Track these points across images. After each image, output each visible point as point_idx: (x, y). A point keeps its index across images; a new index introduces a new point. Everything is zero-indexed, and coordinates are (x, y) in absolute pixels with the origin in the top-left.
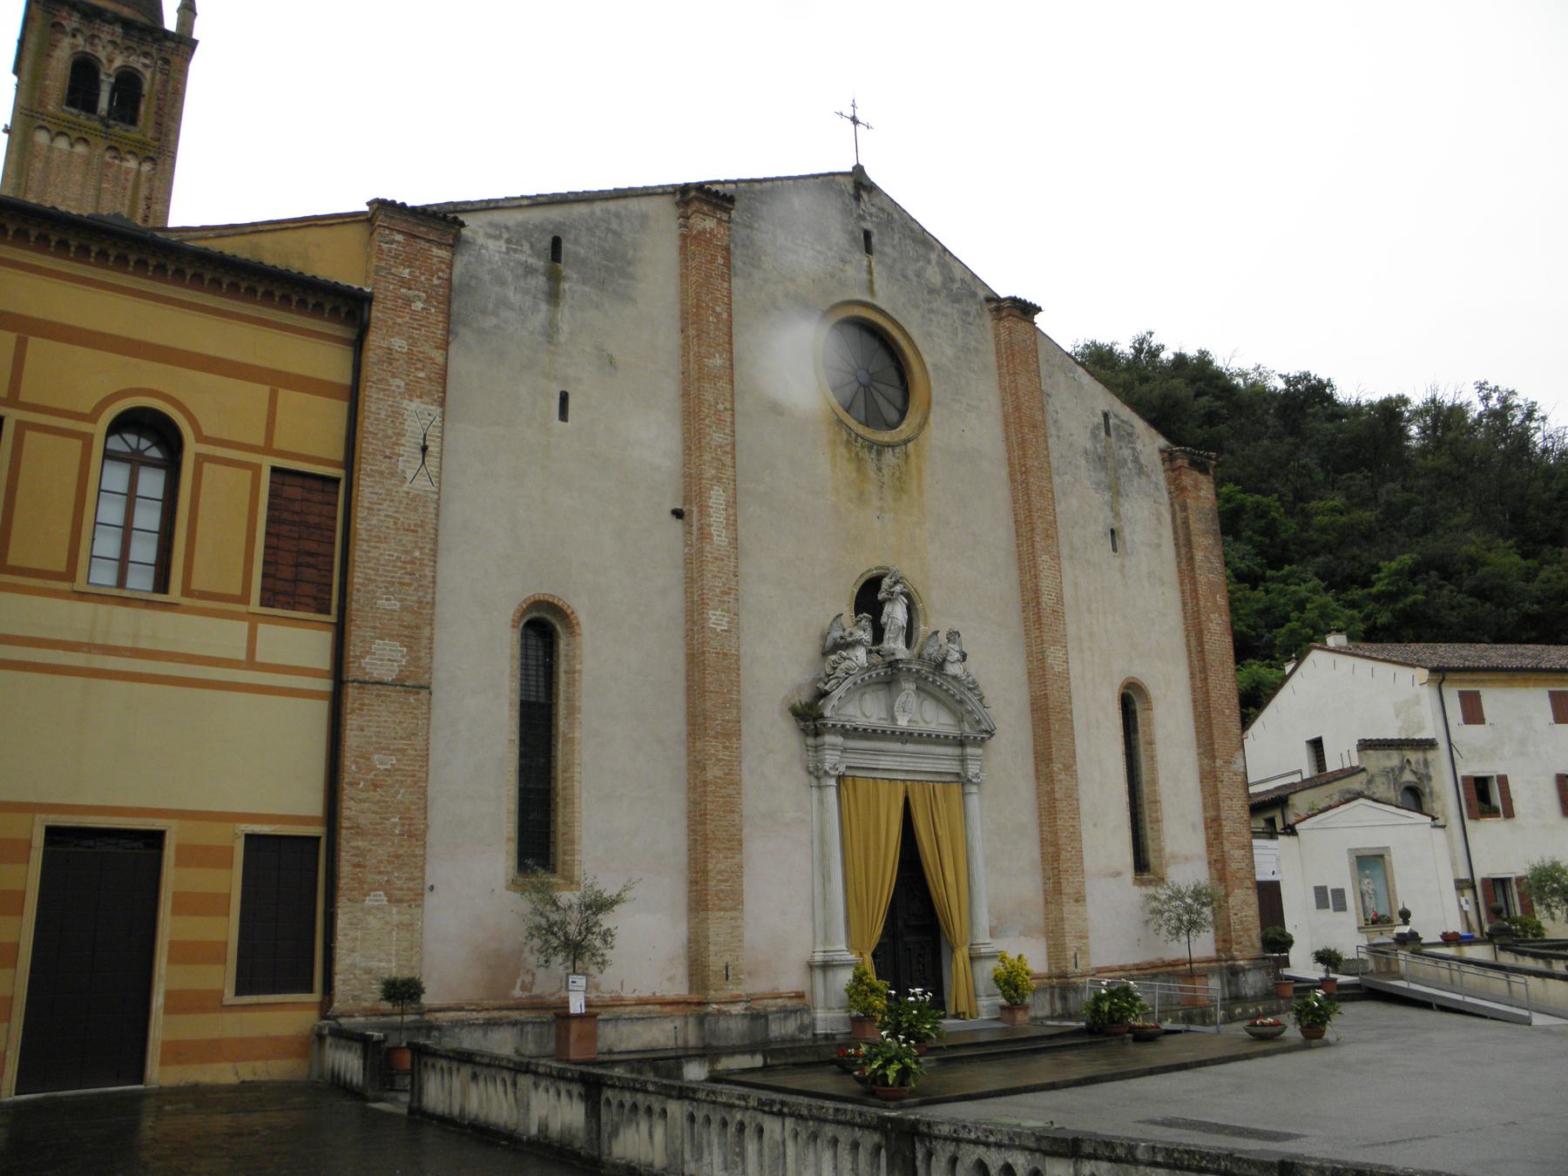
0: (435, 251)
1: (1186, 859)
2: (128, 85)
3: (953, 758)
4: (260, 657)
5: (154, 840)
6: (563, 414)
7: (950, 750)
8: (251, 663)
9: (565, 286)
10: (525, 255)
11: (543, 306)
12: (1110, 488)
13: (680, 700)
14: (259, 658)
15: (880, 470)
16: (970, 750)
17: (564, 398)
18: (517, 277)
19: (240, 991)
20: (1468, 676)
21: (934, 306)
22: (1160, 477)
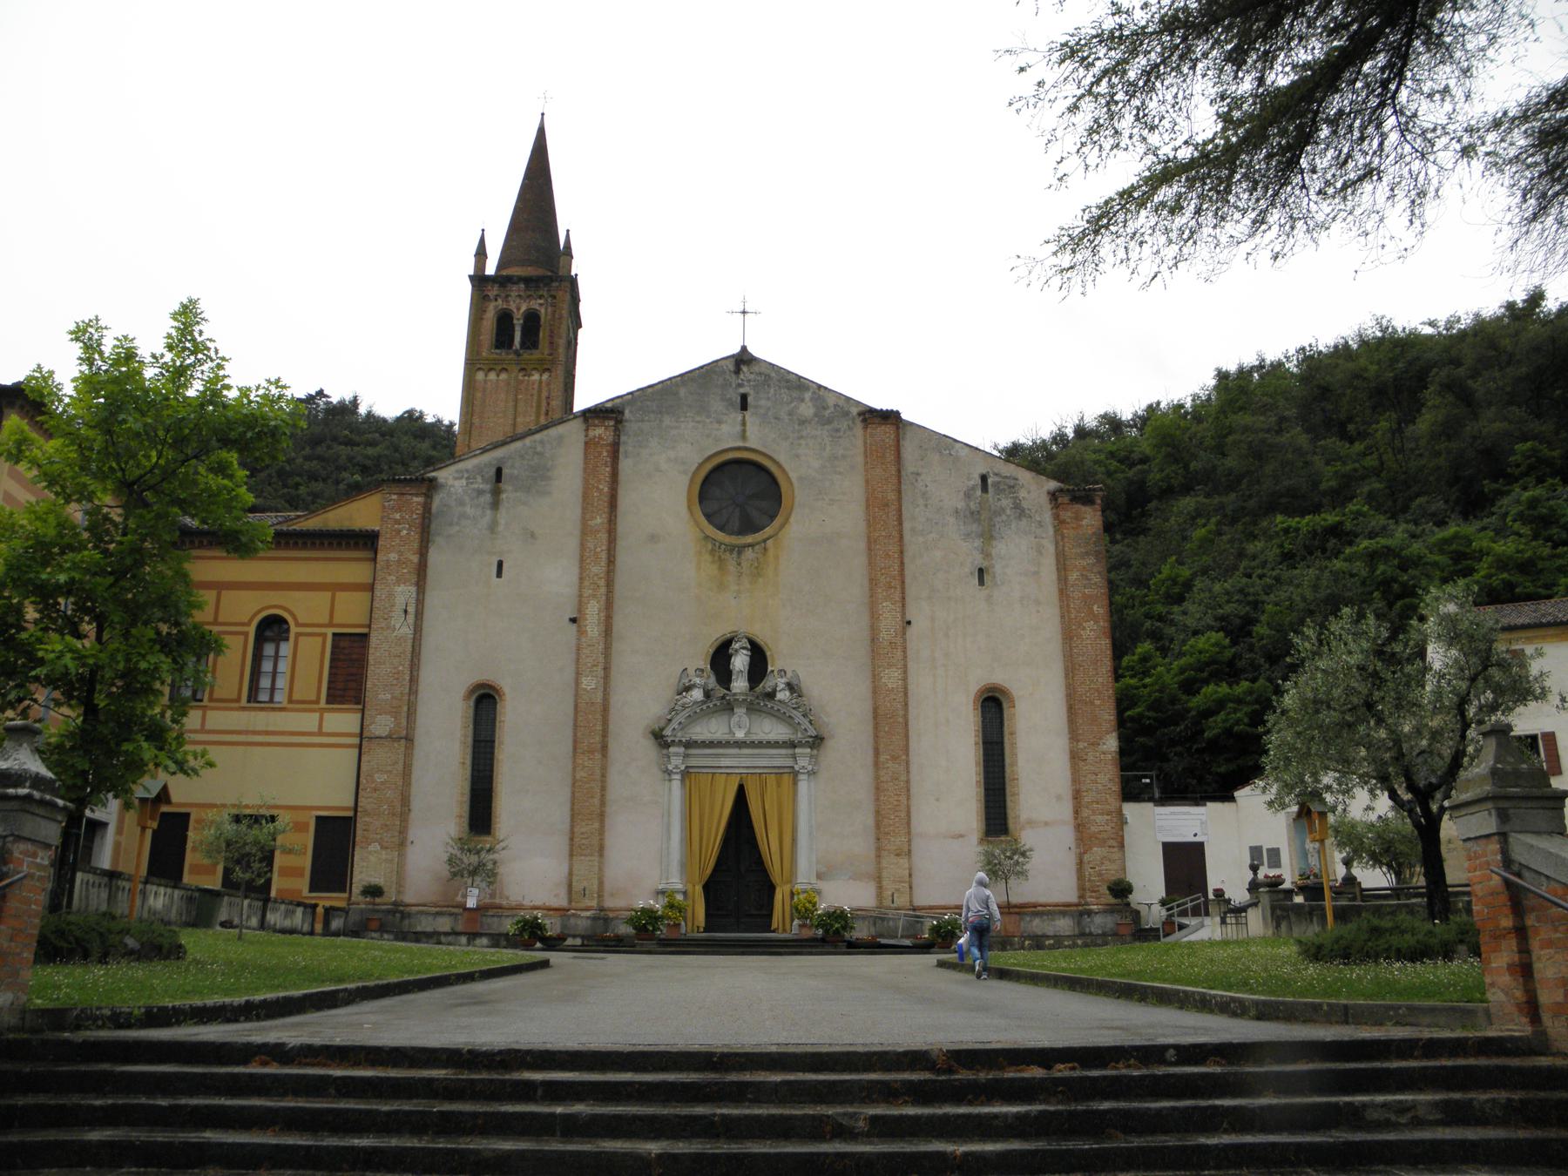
0: (415, 499)
1: (1046, 824)
2: (532, 320)
3: (787, 756)
4: (325, 730)
5: (187, 815)
6: (499, 574)
7: (783, 751)
8: (320, 733)
9: (504, 496)
10: (479, 484)
11: (489, 512)
12: (982, 535)
13: (569, 732)
14: (324, 730)
15: (739, 564)
16: (798, 750)
17: (500, 564)
18: (472, 499)
19: (311, 891)
21: (804, 433)
22: (1047, 516)
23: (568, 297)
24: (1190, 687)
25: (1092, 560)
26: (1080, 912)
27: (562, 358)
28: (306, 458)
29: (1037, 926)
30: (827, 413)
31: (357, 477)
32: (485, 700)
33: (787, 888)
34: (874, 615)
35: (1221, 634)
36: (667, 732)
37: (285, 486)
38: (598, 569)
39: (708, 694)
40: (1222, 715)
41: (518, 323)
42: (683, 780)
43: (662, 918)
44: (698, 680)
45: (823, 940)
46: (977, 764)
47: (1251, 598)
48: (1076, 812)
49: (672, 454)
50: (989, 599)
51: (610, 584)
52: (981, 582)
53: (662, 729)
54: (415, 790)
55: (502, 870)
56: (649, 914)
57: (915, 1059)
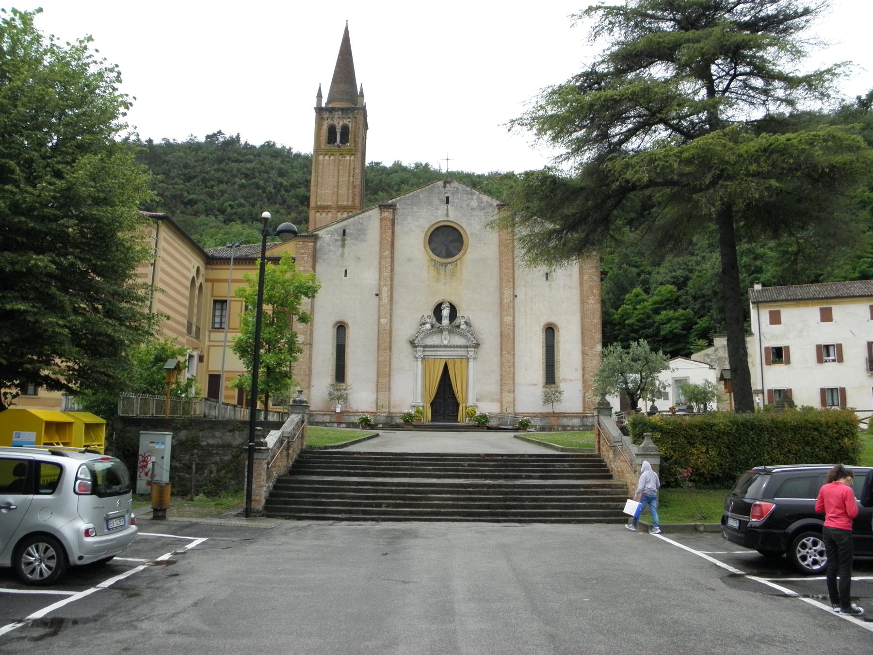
1: (571, 380)
2: (345, 130)
6: (346, 275)
7: (463, 349)
9: (346, 242)
10: (336, 237)
11: (340, 249)
17: (346, 271)
20: (773, 304)
23: (362, 118)
24: (657, 311)
25: (594, 270)
26: (583, 416)
27: (360, 148)
28: (217, 170)
29: (565, 421)
30: (483, 205)
31: (244, 181)
32: (341, 328)
33: (464, 405)
34: (501, 293)
35: (673, 286)
36: (416, 341)
37: (206, 187)
38: (387, 274)
39: (432, 326)
40: (669, 325)
41: (338, 131)
42: (422, 361)
43: (414, 417)
44: (428, 320)
45: (478, 426)
46: (543, 355)
47: (690, 267)
48: (583, 376)
49: (417, 223)
50: (550, 286)
51: (392, 280)
52: (547, 278)
53: (414, 340)
54: (313, 366)
55: (350, 397)
56: (409, 414)
57: (478, 455)
